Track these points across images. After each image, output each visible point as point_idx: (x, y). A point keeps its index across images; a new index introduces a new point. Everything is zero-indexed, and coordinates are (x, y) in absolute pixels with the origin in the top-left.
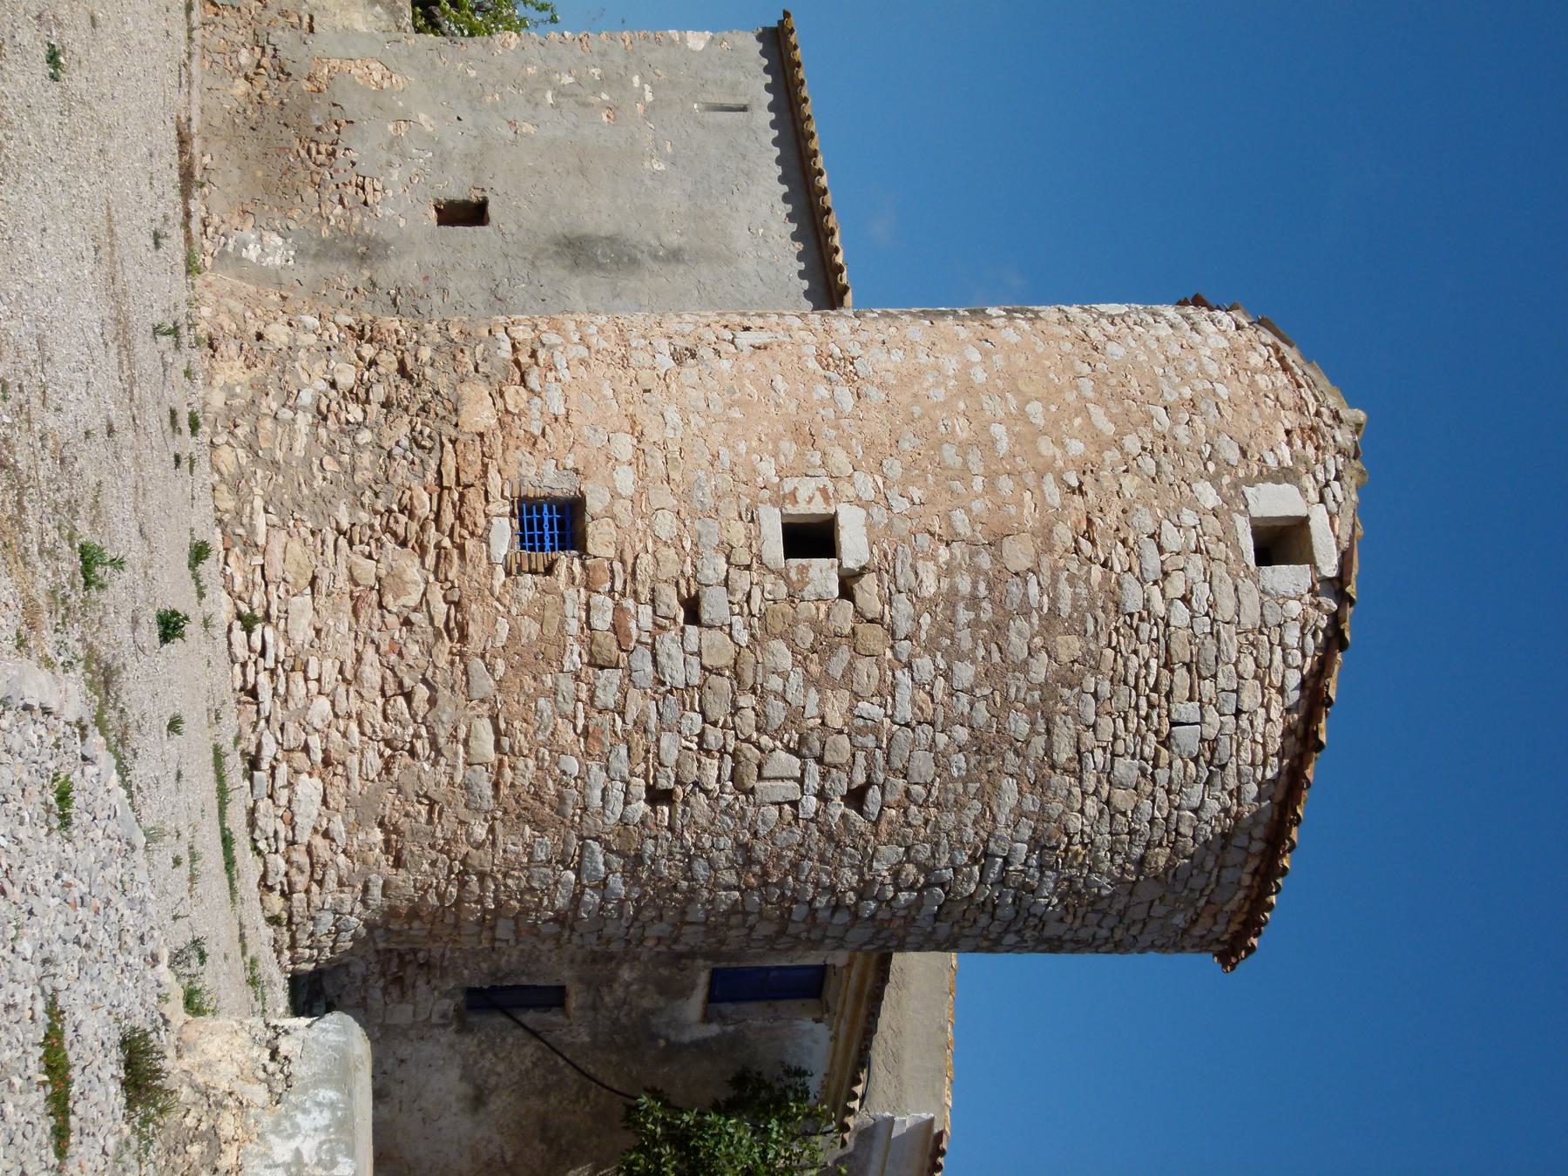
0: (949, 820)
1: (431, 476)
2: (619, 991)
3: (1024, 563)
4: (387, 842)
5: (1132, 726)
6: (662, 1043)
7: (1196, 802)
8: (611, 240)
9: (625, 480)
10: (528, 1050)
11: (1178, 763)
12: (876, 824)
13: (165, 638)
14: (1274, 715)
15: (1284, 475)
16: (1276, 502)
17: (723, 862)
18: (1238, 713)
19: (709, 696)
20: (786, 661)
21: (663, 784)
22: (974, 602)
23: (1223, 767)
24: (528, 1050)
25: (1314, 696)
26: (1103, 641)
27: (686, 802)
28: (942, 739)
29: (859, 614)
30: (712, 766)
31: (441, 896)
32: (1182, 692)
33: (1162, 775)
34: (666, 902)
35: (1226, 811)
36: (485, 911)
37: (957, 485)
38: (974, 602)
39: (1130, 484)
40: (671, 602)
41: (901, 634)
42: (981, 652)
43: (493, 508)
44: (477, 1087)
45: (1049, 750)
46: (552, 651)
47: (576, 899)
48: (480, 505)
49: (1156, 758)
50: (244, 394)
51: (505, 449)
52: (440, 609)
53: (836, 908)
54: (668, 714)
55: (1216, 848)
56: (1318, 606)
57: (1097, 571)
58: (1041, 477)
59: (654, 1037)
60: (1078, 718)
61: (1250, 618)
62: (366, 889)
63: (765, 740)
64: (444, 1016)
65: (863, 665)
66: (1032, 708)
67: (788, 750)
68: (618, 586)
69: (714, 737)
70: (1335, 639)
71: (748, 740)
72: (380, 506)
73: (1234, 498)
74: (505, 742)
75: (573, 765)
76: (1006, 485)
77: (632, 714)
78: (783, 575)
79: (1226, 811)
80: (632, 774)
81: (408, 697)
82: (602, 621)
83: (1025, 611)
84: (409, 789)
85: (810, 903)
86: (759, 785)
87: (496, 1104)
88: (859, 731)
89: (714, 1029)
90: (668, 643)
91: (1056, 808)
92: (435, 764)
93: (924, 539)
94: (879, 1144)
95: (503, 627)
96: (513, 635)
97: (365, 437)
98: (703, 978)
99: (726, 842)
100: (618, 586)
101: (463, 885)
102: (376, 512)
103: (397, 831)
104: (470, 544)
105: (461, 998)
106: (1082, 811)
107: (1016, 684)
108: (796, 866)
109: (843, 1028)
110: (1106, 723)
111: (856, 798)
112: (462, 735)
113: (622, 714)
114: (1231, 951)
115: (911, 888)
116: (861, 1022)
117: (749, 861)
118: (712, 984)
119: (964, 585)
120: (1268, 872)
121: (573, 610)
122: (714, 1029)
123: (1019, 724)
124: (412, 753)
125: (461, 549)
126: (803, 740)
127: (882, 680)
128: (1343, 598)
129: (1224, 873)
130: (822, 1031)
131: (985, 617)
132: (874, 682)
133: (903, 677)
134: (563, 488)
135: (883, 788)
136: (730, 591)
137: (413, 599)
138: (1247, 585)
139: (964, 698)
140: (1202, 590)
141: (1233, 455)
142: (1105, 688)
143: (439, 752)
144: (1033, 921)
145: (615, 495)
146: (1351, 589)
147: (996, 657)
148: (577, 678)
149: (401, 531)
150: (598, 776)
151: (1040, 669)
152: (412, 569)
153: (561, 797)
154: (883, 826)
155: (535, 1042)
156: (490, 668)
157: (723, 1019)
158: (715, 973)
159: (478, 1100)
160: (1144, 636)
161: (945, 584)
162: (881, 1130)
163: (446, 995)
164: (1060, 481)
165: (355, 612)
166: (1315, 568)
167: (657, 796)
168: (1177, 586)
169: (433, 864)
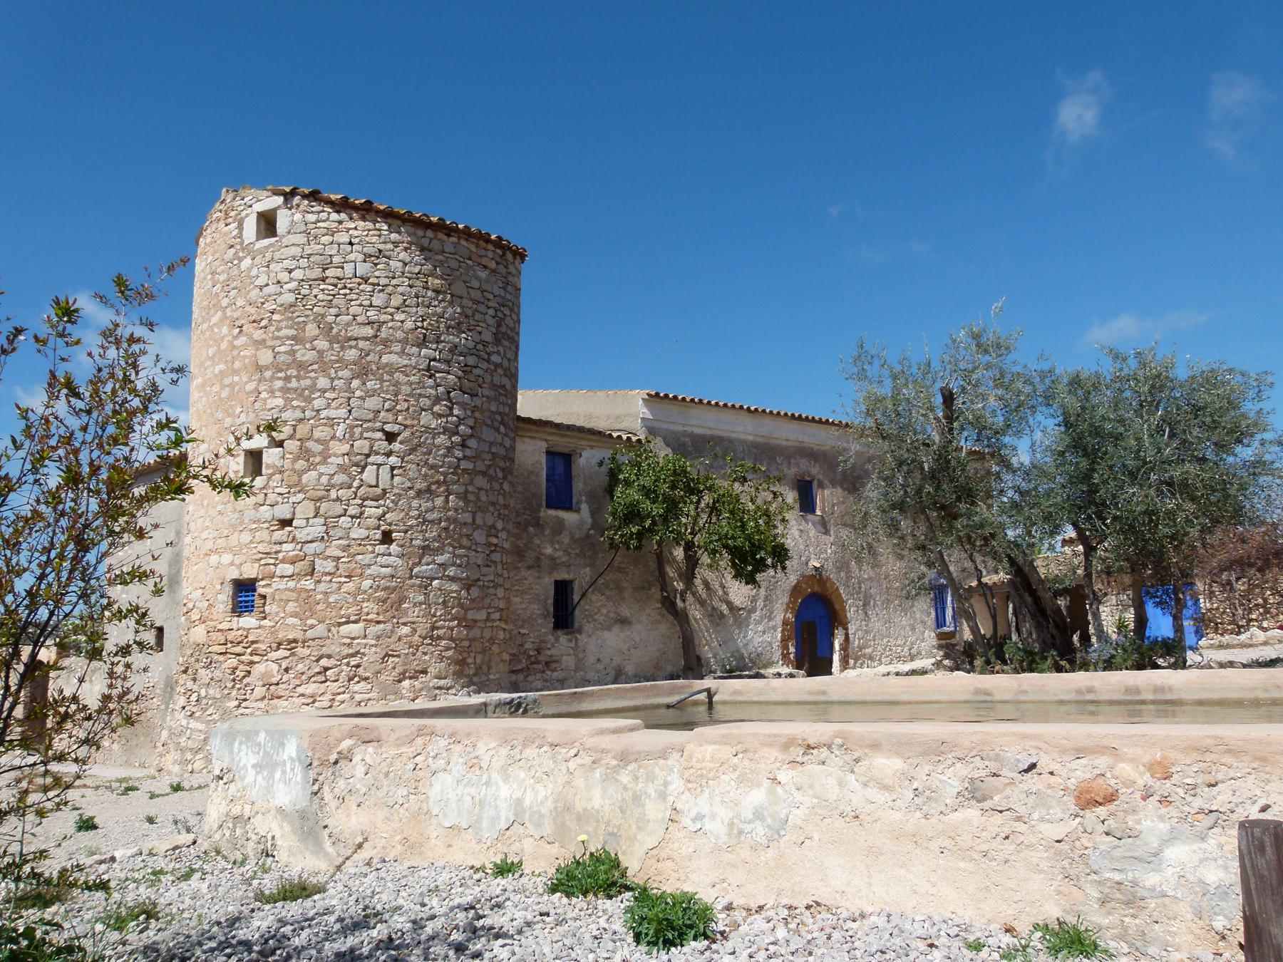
0: (405, 389)
1: (221, 658)
2: (559, 554)
3: (270, 354)
4: (410, 678)
5: (355, 297)
6: (592, 532)
7: (400, 264)
8: (170, 566)
9: (227, 558)
10: (594, 598)
11: (377, 274)
12: (406, 426)
13: (95, 827)
14: (353, 225)
15: (240, 227)
16: (251, 225)
17: (429, 504)
18: (351, 244)
19: (330, 513)
20: (313, 474)
21: (379, 535)
22: (287, 379)
23: (380, 251)
24: (594, 598)
25: (343, 206)
26: (309, 312)
27: (390, 524)
28: (358, 393)
29: (291, 437)
30: (368, 511)
31: (447, 649)
32: (339, 272)
33: (383, 281)
34: (453, 533)
35: (406, 249)
36: (459, 625)
37: (236, 389)
38: (287, 379)
39: (240, 302)
40: (280, 535)
41: (302, 416)
42: (313, 374)
43: (235, 627)
44: (616, 622)
45: (366, 339)
46: (304, 595)
47: (452, 579)
48: (233, 633)
49: (374, 284)
50: (178, 756)
51: (212, 620)
52: (282, 653)
53: (463, 445)
54: (339, 535)
55: (429, 254)
56: (298, 206)
57: (276, 317)
58: (234, 347)
59: (588, 536)
60: (348, 324)
61: (301, 239)
62: (440, 688)
63: (355, 484)
64: (570, 641)
65: (317, 434)
66: (343, 348)
67: (362, 471)
68: (272, 561)
69: (353, 510)
70: (314, 196)
71: (356, 494)
72: (230, 685)
73: (248, 249)
74: (353, 618)
75: (367, 584)
76: (237, 365)
77: (339, 553)
78: (270, 477)
79: (406, 249)
80: (373, 552)
81: (326, 669)
82: (288, 569)
83: (292, 353)
84: (378, 668)
85: (459, 460)
86: (381, 486)
87: (625, 612)
88: (352, 436)
89: (584, 507)
90: (301, 535)
91: (399, 335)
92: (364, 654)
93: (257, 405)
94: (657, 425)
95: (291, 621)
96: (295, 615)
97: (203, 693)
98: (552, 512)
99: (415, 503)
100: (272, 561)
101: (439, 638)
102: (233, 687)
103: (404, 673)
104: (251, 638)
105: (559, 633)
106: (402, 322)
107: (330, 356)
108: (432, 467)
109: (583, 443)
110: (352, 310)
111: (390, 437)
112: (348, 641)
113: (339, 558)
114: (520, 255)
115: (451, 409)
116: (574, 434)
117: (428, 490)
118: (556, 508)
119: (279, 384)
120: (441, 227)
121: (282, 585)
122: (584, 507)
123: (352, 354)
124: (358, 666)
125: (253, 642)
126: (357, 465)
127: (325, 425)
128: (293, 193)
129: (447, 250)
130: (586, 454)
131: (295, 373)
132: (326, 429)
133: (324, 414)
134: (229, 590)
135: (385, 423)
136: (277, 503)
137: (275, 667)
138: (285, 241)
139: (336, 382)
140: (287, 264)
141: (233, 251)
142: (333, 311)
143: (358, 652)
144: (480, 347)
145: (232, 564)
146: (288, 190)
147: (315, 367)
148: (319, 582)
149: (242, 674)
150: (374, 570)
151: (322, 344)
152: (259, 669)
153: (385, 589)
154: (408, 422)
155: (589, 594)
156: (312, 627)
157: (579, 502)
158: (549, 506)
159: (624, 622)
160: (307, 292)
161: (278, 394)
162: (649, 424)
163: (557, 639)
164: (236, 338)
165: (279, 697)
166: (279, 207)
167: (387, 538)
168: (284, 276)
169: (425, 654)
